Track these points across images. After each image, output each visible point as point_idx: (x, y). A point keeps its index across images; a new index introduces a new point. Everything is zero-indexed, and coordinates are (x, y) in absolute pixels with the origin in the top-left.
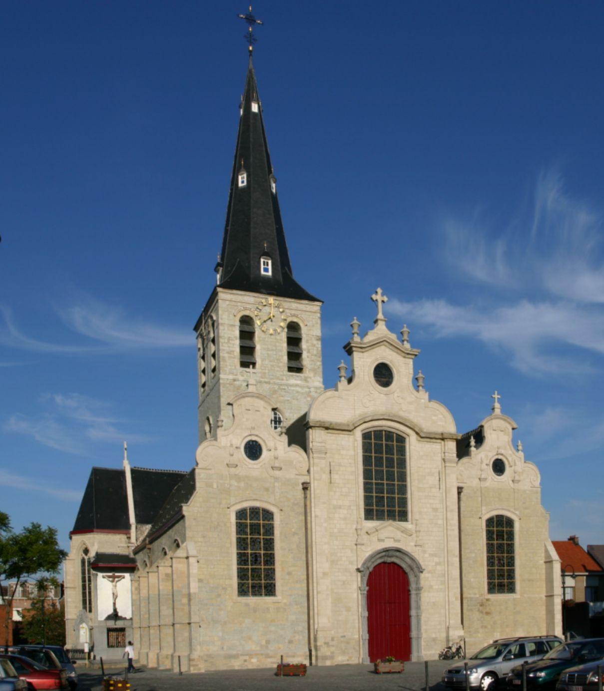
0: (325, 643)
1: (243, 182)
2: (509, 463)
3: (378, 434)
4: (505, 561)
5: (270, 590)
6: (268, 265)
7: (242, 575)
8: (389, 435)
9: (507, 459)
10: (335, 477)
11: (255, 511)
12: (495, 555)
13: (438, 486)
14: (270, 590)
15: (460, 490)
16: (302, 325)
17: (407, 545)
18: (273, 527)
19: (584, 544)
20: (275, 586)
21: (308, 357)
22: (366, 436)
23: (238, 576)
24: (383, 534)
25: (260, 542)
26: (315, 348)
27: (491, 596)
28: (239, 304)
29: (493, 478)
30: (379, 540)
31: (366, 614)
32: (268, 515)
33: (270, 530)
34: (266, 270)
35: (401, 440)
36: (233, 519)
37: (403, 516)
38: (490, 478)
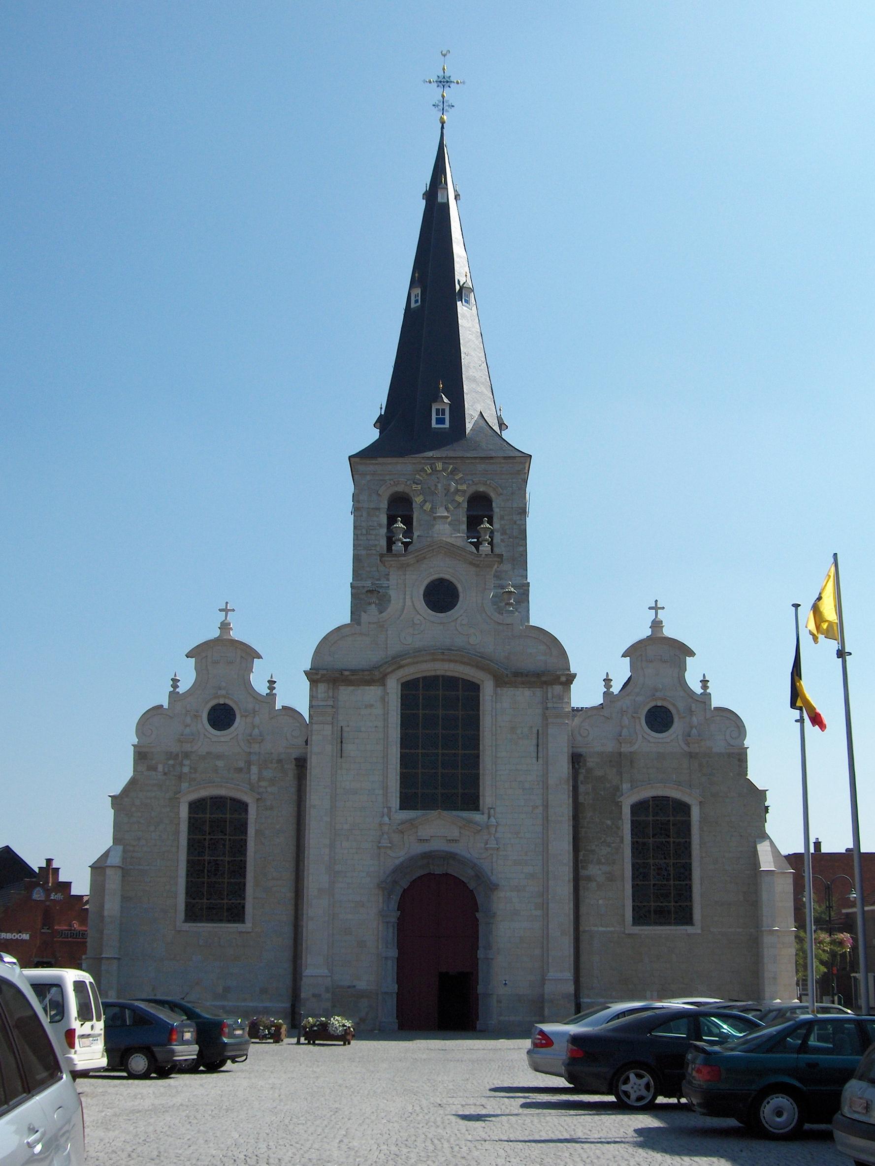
0: (314, 995)
1: (416, 301)
2: (678, 711)
3: (431, 682)
4: (672, 873)
5: (237, 914)
6: (443, 414)
7: (192, 891)
8: (451, 682)
9: (674, 705)
10: (349, 748)
11: (218, 802)
12: (651, 861)
13: (535, 755)
14: (237, 914)
15: (576, 759)
16: (493, 495)
17: (470, 847)
18: (246, 824)
19: (74, 891)
20: (243, 907)
21: (502, 541)
22: (409, 688)
23: (187, 893)
24: (425, 831)
25: (224, 845)
26: (515, 527)
27: (637, 929)
28: (387, 477)
29: (646, 736)
30: (421, 840)
31: (394, 953)
32: (242, 807)
33: (242, 828)
34: (440, 421)
35: (474, 688)
36: (184, 812)
37: (401, 809)
38: (640, 737)
